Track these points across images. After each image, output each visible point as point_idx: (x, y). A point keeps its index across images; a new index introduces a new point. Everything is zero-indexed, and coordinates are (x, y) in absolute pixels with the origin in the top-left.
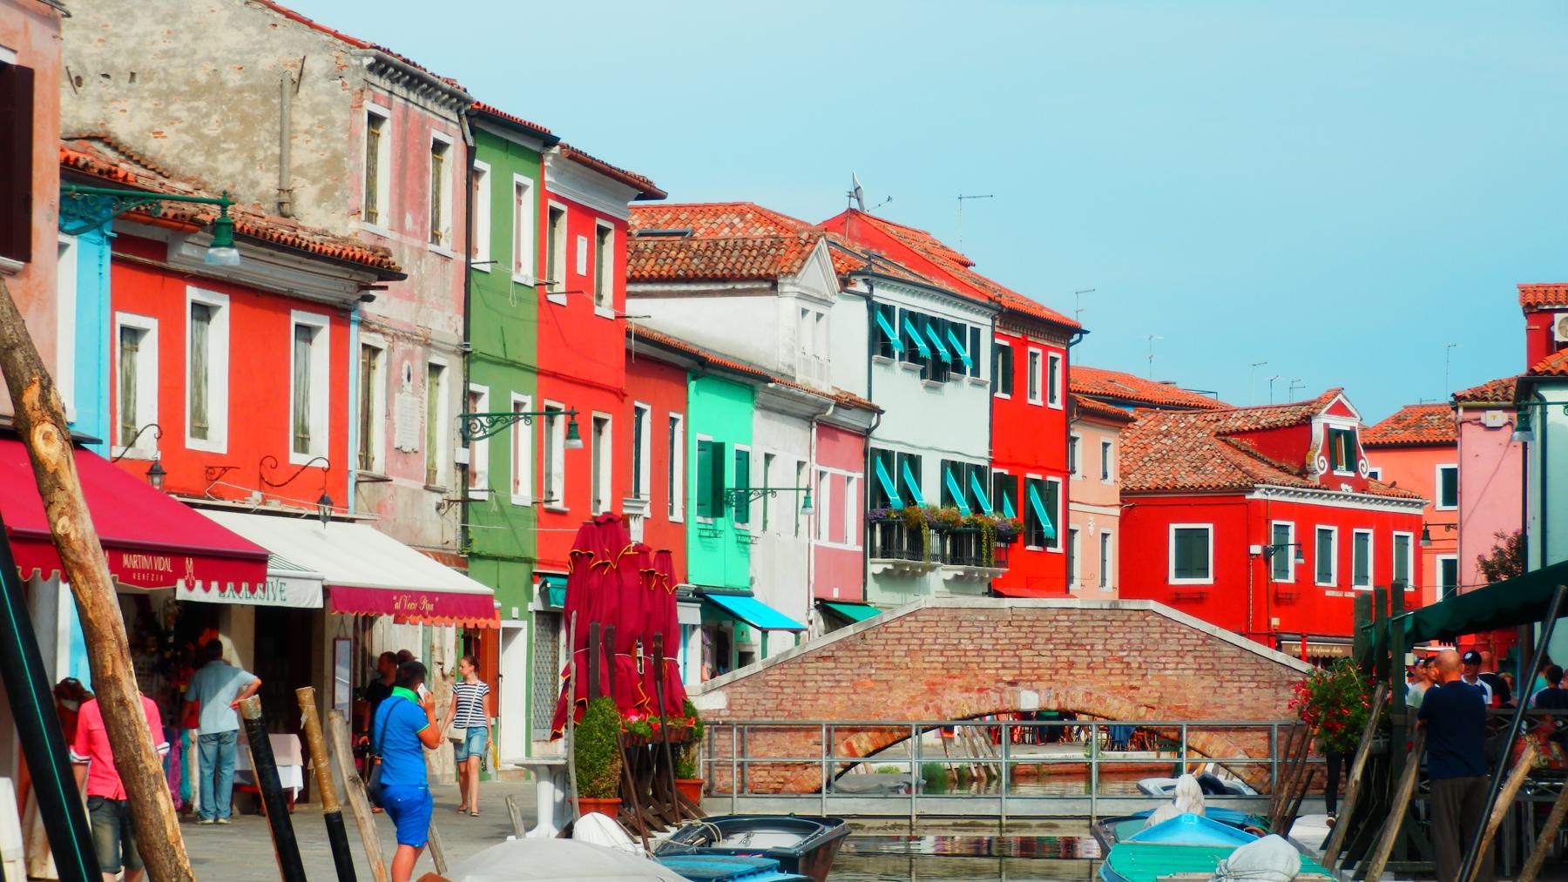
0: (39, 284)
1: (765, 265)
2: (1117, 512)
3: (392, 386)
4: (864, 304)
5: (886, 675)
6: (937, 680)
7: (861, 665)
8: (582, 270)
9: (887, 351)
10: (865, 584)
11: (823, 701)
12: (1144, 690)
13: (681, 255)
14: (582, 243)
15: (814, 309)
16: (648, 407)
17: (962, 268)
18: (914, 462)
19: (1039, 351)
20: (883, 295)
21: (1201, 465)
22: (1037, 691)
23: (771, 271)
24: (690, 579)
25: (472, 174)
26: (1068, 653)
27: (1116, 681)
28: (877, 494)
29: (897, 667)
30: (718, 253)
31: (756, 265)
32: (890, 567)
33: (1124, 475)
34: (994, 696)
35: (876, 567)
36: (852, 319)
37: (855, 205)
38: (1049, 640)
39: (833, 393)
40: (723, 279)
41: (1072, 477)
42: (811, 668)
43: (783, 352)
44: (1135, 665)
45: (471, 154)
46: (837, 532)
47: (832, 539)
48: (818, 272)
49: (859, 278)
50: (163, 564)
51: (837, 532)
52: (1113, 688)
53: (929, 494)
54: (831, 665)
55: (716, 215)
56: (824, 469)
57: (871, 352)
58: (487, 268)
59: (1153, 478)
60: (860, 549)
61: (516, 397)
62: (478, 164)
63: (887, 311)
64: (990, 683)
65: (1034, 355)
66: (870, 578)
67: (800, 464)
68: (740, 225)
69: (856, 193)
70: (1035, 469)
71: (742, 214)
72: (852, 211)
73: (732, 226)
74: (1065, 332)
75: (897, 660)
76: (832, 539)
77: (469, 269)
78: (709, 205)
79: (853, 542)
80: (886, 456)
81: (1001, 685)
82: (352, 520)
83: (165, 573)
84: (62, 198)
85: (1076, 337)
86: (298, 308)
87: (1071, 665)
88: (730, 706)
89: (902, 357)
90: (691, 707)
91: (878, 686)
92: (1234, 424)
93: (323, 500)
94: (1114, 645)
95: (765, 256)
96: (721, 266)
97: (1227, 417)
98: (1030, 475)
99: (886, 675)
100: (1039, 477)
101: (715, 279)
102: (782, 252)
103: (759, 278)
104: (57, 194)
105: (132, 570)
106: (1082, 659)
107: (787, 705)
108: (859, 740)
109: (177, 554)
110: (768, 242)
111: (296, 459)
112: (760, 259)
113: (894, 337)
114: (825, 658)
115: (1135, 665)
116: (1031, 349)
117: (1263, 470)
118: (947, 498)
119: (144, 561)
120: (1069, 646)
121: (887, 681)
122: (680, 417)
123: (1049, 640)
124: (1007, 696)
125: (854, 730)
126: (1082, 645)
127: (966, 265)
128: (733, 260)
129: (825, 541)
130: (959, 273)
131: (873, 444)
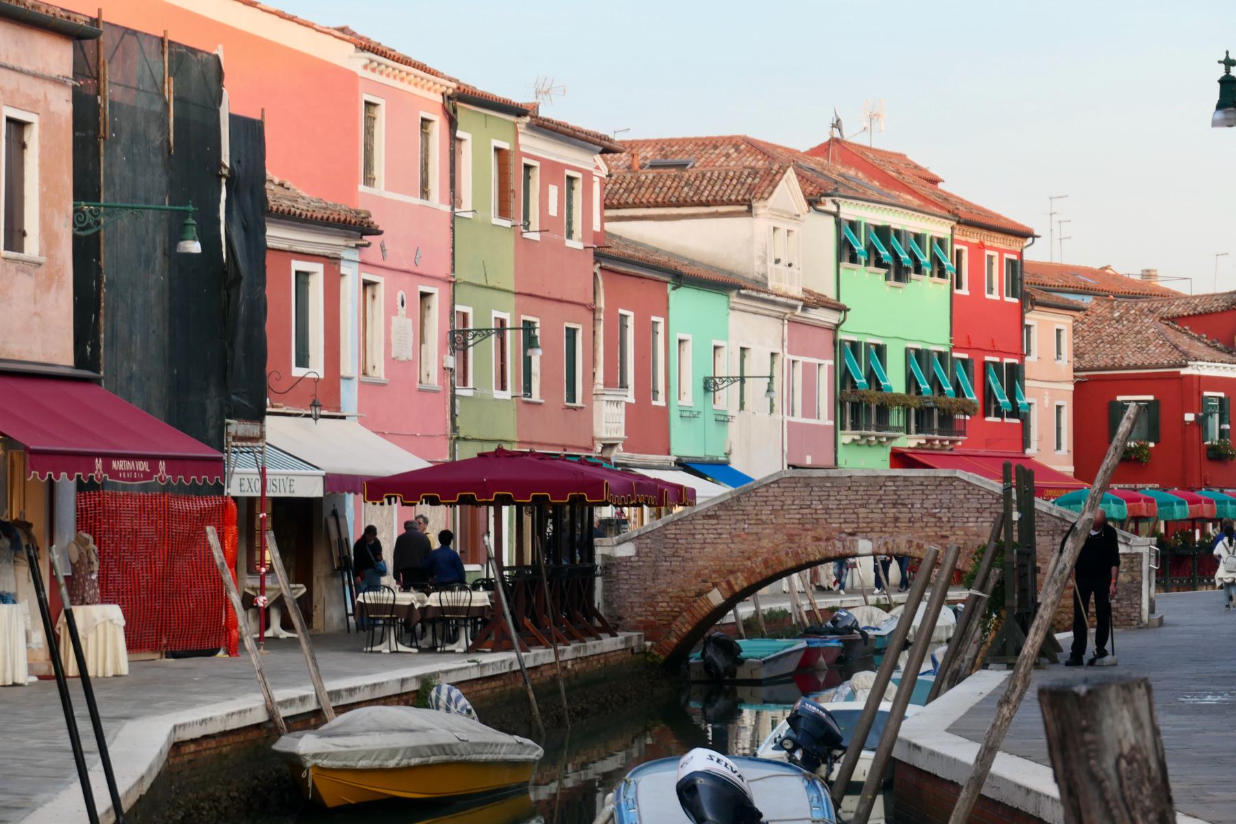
0: (59, 270)
1: (742, 192)
2: (1071, 387)
3: (390, 311)
4: (832, 219)
5: (755, 529)
6: (795, 532)
7: (737, 521)
8: (553, 211)
9: (854, 259)
10: (836, 452)
11: (708, 549)
12: (953, 538)
13: (675, 184)
14: (553, 191)
15: (784, 227)
16: (631, 314)
17: (929, 185)
18: (880, 351)
19: (996, 254)
20: (850, 211)
21: (1146, 348)
22: (871, 540)
23: (747, 197)
24: (673, 452)
25: (454, 140)
26: (894, 510)
27: (930, 531)
28: (844, 378)
29: (763, 523)
30: (705, 182)
31: (735, 192)
32: (857, 437)
33: (1078, 354)
34: (839, 544)
35: (846, 437)
36: (823, 232)
37: (837, 134)
38: (880, 500)
39: (801, 295)
40: (707, 204)
41: (1027, 359)
42: (699, 522)
43: (757, 263)
44: (945, 519)
45: (452, 123)
46: (810, 409)
47: (804, 416)
48: (789, 191)
49: (828, 199)
50: (143, 466)
51: (810, 409)
52: (929, 536)
53: (895, 381)
54: (715, 521)
55: (715, 147)
56: (821, 361)
57: (839, 259)
58: (470, 215)
59: (1102, 358)
60: (832, 423)
61: (496, 314)
62: (459, 134)
63: (853, 225)
64: (835, 534)
65: (990, 257)
66: (840, 447)
67: (773, 354)
68: (735, 155)
69: (837, 125)
70: (992, 352)
71: (737, 147)
72: (837, 140)
73: (728, 156)
74: (1024, 234)
75: (764, 517)
76: (804, 416)
77: (454, 218)
78: (710, 139)
79: (825, 418)
80: (855, 346)
81: (843, 535)
82: (343, 417)
83: (144, 472)
84: (75, 212)
85: (1030, 240)
86: (297, 259)
87: (896, 519)
88: (638, 554)
89: (867, 263)
90: (616, 558)
91: (751, 538)
92: (1175, 310)
93: (314, 405)
94: (928, 504)
95: (743, 184)
96: (706, 193)
97: (1170, 304)
98: (988, 358)
99: (755, 529)
100: (997, 359)
101: (701, 204)
102: (757, 181)
103: (737, 203)
104: (71, 208)
105: (118, 471)
106: (904, 515)
107: (682, 553)
108: (736, 579)
109: (153, 460)
110: (746, 173)
111: (297, 372)
112: (739, 187)
113: (860, 248)
114: (710, 517)
115: (945, 519)
116: (988, 252)
117: (1198, 348)
118: (910, 379)
119: (129, 465)
120: (895, 505)
121: (757, 534)
122: (661, 320)
123: (880, 500)
124: (848, 544)
125: (732, 572)
126: (904, 505)
127: (934, 181)
128: (717, 188)
129: (798, 418)
130: (926, 190)
131: (842, 336)
